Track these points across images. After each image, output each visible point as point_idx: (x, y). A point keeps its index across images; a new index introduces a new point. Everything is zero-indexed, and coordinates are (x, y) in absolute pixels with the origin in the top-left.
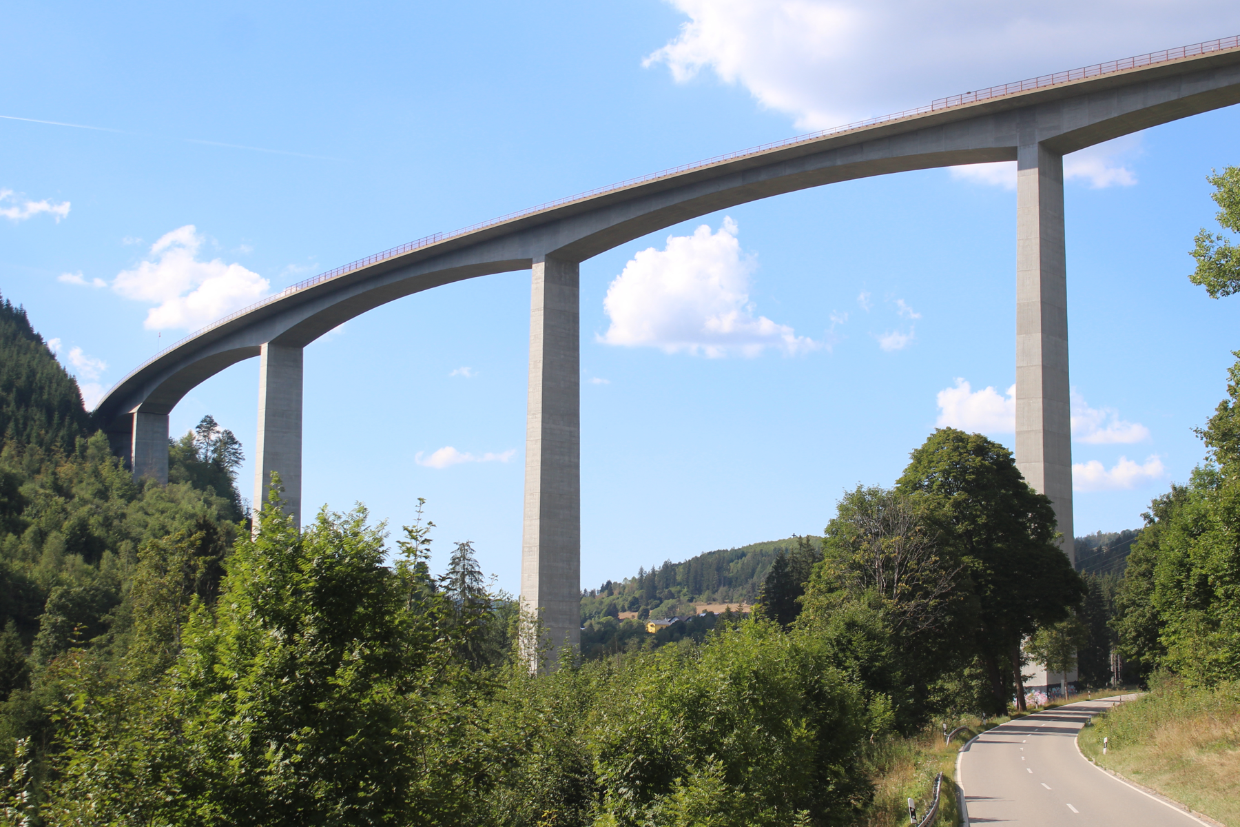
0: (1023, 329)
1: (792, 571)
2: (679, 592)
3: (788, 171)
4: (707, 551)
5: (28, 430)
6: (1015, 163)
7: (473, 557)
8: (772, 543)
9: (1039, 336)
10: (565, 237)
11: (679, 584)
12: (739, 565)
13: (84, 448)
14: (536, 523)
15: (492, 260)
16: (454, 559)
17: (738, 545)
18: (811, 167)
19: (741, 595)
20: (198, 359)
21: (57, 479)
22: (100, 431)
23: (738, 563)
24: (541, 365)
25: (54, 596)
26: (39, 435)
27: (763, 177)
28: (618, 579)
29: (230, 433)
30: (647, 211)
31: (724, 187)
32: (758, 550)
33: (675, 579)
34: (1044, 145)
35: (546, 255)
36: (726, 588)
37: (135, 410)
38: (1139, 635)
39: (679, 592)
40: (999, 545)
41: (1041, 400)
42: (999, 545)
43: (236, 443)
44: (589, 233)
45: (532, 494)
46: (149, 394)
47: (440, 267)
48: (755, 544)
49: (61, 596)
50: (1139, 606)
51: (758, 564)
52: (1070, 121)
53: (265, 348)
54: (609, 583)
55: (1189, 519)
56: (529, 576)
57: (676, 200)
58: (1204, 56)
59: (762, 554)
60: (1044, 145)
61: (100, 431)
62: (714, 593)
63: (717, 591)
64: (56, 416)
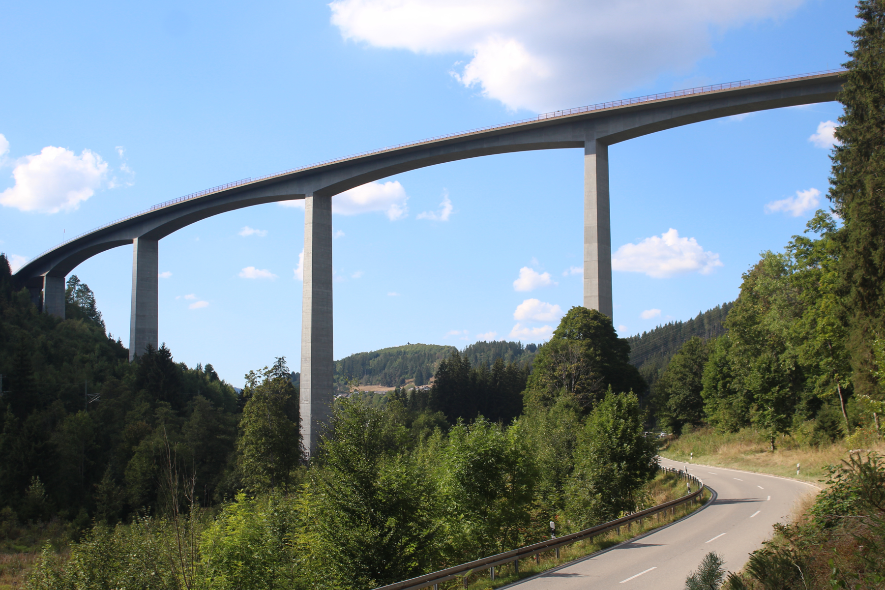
0: (587, 241)
1: (449, 371)
2: (338, 378)
3: (456, 150)
4: (355, 353)
6: (583, 149)
7: (285, 365)
9: (596, 245)
10: (325, 183)
11: (338, 373)
12: (376, 362)
14: (310, 345)
15: (281, 194)
17: (374, 349)
18: (469, 148)
19: (378, 380)
20: (90, 246)
23: (374, 360)
24: (311, 255)
27: (442, 153)
29: (86, 285)
31: (419, 157)
32: (387, 352)
33: (335, 371)
34: (598, 140)
35: (314, 193)
36: (368, 376)
37: (44, 275)
38: (678, 407)
39: (338, 378)
40: (606, 364)
41: (597, 280)
42: (606, 364)
43: (90, 291)
44: (339, 181)
45: (306, 328)
46: (55, 265)
47: (248, 197)
48: (385, 349)
50: (677, 394)
51: (388, 361)
53: (136, 240)
55: (717, 359)
56: (305, 375)
58: (685, 97)
59: (390, 355)
60: (598, 140)
62: (360, 379)
63: (362, 378)
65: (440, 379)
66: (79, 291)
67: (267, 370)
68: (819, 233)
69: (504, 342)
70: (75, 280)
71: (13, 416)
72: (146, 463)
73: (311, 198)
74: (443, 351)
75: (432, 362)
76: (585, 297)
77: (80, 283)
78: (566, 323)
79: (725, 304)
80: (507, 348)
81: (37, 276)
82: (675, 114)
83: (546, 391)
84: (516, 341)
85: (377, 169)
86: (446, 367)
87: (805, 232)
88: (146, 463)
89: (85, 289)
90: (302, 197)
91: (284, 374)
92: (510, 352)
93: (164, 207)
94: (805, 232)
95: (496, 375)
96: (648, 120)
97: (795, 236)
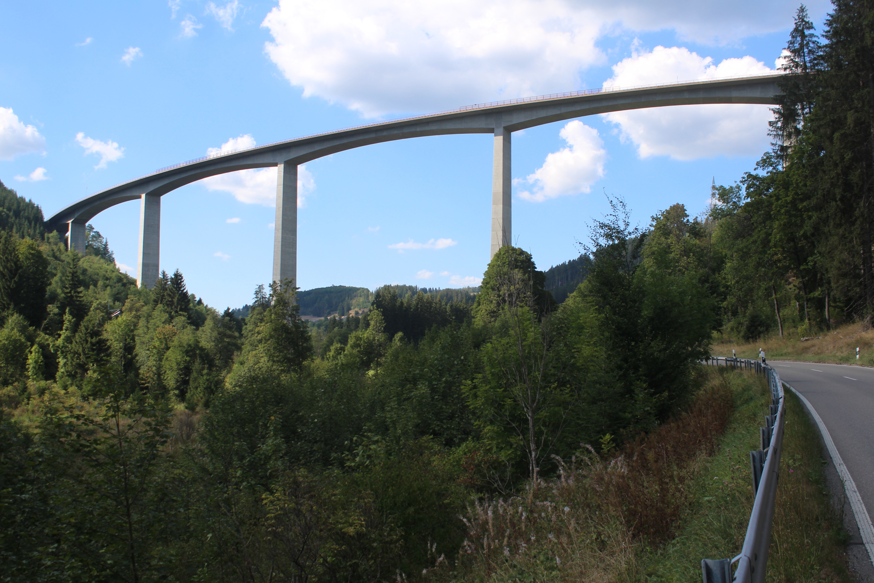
0: (495, 203)
3: (396, 132)
5: (22, 229)
7: (264, 291)
8: (412, 290)
9: (501, 206)
10: (293, 154)
13: (48, 238)
16: (256, 292)
18: (406, 130)
21: (54, 253)
22: (55, 231)
25: (95, 305)
26: (28, 232)
27: (385, 133)
28: (205, 302)
30: (332, 145)
37: (70, 222)
49: (98, 304)
52: (516, 119)
53: (143, 196)
54: (246, 305)
57: (345, 141)
61: (55, 231)
64: (33, 223)
65: (771, 180)
66: (93, 236)
67: (287, 281)
68: (765, 171)
69: (405, 285)
70: (91, 228)
71: (71, 317)
72: (180, 355)
73: (282, 166)
74: (359, 291)
75: (351, 299)
76: (492, 245)
77: (94, 230)
78: (498, 257)
79: (570, 261)
80: (407, 290)
81: (64, 222)
82: (564, 110)
83: (493, 306)
84: (414, 285)
85: (334, 145)
86: (380, 297)
87: (755, 169)
88: (180, 355)
89: (98, 235)
90: (275, 165)
91: (263, 298)
92: (409, 293)
93: (167, 170)
94: (755, 169)
95: (418, 304)
96: (542, 114)
97: (747, 173)
